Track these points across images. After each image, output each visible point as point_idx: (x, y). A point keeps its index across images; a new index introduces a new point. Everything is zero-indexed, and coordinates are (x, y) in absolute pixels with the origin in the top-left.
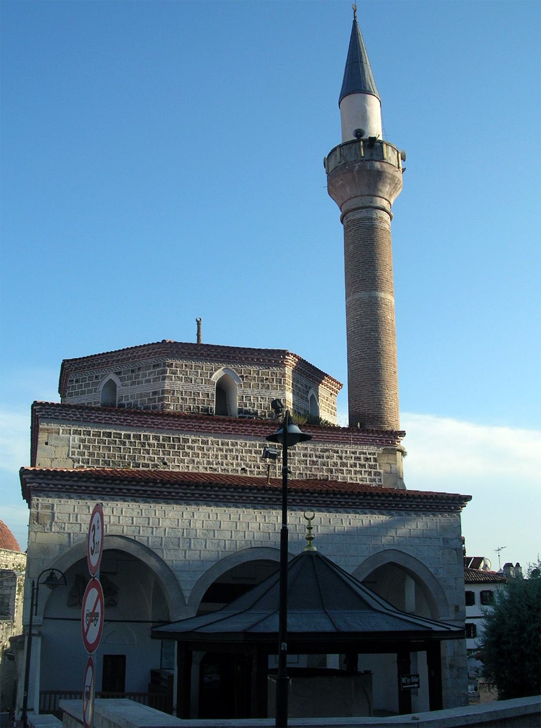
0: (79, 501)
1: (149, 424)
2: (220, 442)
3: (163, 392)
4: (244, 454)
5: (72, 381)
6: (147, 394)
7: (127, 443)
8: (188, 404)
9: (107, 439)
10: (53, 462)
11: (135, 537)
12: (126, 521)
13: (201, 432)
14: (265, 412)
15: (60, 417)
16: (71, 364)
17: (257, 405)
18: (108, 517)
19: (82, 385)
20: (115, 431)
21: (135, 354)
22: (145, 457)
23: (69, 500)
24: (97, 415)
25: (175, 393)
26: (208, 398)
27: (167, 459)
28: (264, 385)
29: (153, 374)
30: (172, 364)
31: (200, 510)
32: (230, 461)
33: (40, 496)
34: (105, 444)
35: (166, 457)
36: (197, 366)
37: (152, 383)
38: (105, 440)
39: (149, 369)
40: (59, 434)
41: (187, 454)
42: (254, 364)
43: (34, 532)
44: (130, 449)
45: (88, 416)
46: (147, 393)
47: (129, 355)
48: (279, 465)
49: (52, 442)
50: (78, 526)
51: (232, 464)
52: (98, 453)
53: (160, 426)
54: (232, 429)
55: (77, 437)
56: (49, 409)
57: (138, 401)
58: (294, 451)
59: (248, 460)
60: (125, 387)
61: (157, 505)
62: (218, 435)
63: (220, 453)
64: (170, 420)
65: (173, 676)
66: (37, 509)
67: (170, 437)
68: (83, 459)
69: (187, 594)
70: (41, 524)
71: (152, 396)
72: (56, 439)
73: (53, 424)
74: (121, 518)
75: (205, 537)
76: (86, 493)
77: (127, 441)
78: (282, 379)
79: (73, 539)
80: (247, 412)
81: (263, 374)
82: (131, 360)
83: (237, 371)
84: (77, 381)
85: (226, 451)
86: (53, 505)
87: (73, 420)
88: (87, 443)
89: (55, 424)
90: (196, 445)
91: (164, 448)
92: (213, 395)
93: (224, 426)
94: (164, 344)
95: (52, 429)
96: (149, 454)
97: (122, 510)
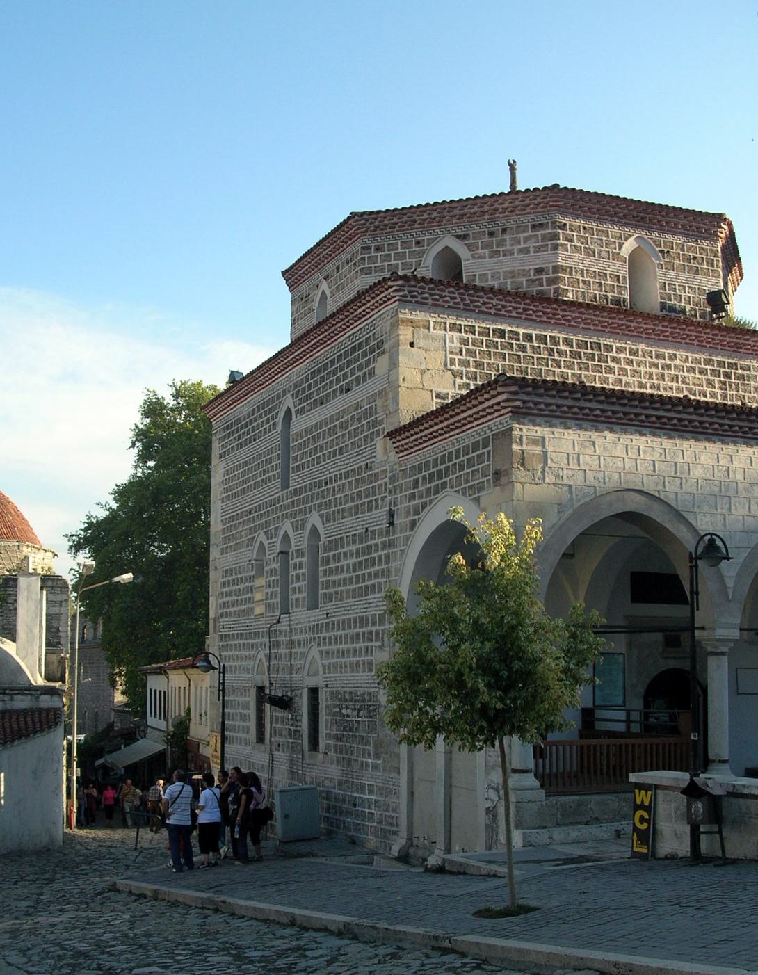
0: (578, 432)
1: (559, 319)
2: (654, 353)
3: (557, 269)
4: (686, 374)
5: (369, 248)
6: (525, 273)
7: (528, 348)
8: (592, 291)
9: (499, 340)
10: (424, 376)
11: (658, 492)
13: (628, 335)
14: (695, 310)
15: (430, 301)
16: (367, 220)
17: (685, 299)
18: (622, 459)
19: (390, 255)
20: (510, 329)
21: (496, 205)
22: (554, 372)
23: (566, 431)
24: (486, 300)
25: (574, 273)
26: (619, 282)
27: (586, 376)
28: (691, 268)
29: (534, 240)
30: (565, 224)
31: (740, 452)
32: (669, 383)
33: (524, 424)
34: (497, 349)
35: (584, 373)
36: (599, 230)
37: (532, 254)
38: (497, 342)
39: (524, 232)
40: (429, 329)
41: (611, 370)
42: (676, 232)
43: (520, 483)
44: (533, 357)
45: (472, 301)
46: (524, 270)
47: (486, 208)
48: (731, 392)
49: (420, 342)
50: (581, 473)
51: (671, 389)
52: (488, 364)
53: (573, 323)
54: (672, 333)
55: (456, 335)
56: (416, 286)
57: (506, 283)
58: (748, 372)
59: (691, 383)
60: (480, 260)
61: (684, 442)
62: (651, 342)
63: (654, 370)
64: (588, 314)
66: (522, 446)
67: (586, 342)
68: (467, 372)
69: (730, 583)
70: (529, 470)
71: (534, 275)
72: (426, 337)
73: (418, 313)
74: (638, 462)
75: (749, 495)
76: (587, 420)
77: (528, 344)
78: (715, 259)
79: (577, 495)
80: (672, 309)
81: (690, 249)
82: (487, 216)
83: (654, 242)
84: (378, 249)
85: (663, 368)
86: (543, 438)
87: (449, 307)
88: (470, 347)
89: (423, 313)
90: (622, 356)
91: (580, 358)
92: (624, 278)
93: (660, 328)
94: (556, 190)
95: (418, 321)
96: (560, 367)
97: (639, 449)
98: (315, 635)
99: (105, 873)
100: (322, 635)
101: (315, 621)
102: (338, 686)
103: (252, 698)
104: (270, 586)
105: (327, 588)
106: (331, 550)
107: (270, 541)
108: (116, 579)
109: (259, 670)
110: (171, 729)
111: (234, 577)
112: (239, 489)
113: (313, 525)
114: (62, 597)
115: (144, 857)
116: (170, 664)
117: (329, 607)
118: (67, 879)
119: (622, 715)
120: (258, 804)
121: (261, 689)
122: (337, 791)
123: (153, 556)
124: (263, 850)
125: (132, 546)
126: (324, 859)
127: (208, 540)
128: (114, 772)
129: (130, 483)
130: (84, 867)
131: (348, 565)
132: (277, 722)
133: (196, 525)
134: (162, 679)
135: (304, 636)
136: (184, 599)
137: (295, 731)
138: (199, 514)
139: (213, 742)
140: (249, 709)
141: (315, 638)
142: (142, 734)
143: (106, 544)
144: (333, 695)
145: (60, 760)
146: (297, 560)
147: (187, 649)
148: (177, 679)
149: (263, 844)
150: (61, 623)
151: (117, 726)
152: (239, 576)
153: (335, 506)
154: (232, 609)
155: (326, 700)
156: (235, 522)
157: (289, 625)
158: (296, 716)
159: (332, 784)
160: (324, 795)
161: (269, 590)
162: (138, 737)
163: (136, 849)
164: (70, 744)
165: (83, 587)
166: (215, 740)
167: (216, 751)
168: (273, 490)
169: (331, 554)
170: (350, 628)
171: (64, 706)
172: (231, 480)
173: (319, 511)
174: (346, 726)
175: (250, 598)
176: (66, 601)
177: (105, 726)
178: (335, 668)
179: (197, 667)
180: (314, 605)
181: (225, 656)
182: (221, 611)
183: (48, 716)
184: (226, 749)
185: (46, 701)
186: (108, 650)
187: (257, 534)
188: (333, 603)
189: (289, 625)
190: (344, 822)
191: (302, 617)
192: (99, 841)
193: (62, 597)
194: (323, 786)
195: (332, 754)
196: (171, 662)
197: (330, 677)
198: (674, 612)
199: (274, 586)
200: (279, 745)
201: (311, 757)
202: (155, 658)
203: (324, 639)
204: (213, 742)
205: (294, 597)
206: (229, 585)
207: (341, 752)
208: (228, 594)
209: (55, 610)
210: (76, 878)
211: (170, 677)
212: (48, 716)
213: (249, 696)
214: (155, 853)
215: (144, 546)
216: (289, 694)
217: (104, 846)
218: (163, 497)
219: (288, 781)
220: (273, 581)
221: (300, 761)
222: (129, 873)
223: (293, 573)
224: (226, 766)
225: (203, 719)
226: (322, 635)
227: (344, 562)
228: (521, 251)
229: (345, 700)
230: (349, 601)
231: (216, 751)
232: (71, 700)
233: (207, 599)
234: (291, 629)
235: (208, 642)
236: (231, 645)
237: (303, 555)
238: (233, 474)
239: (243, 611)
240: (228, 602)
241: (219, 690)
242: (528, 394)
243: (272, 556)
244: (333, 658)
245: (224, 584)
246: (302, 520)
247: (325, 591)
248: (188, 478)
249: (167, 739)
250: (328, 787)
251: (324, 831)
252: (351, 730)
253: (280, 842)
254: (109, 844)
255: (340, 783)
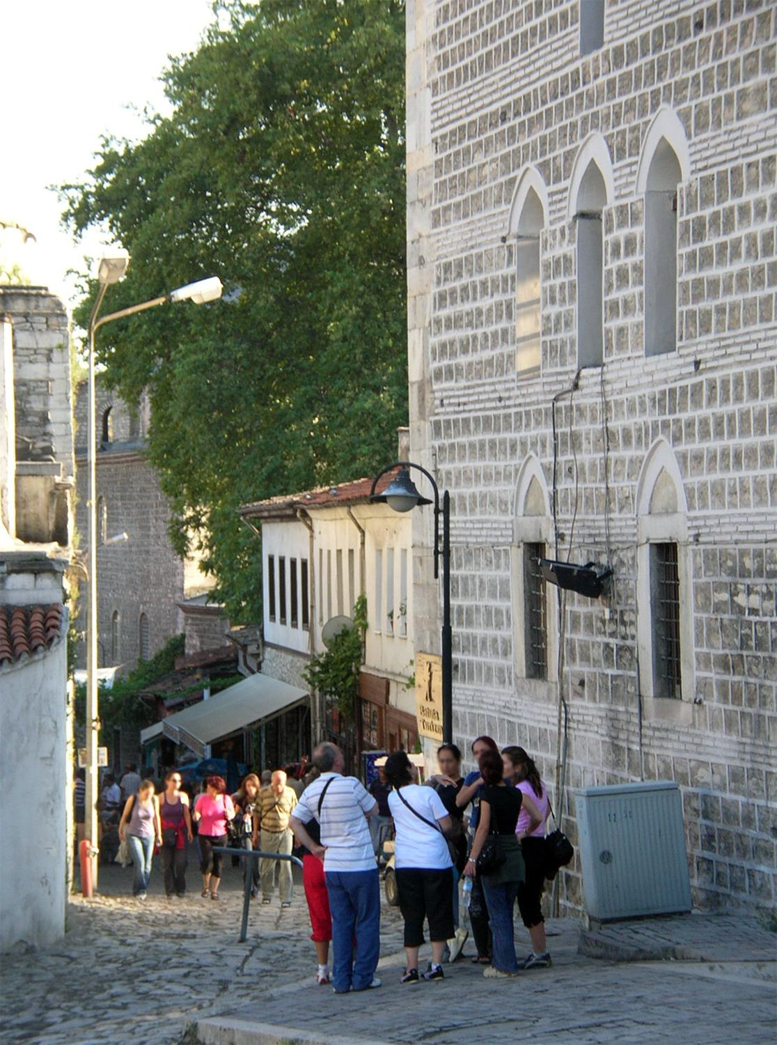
98: (667, 417)
99: (168, 1001)
100: (683, 416)
101: (666, 381)
102: (728, 538)
103: (513, 571)
104: (553, 301)
105: (697, 298)
106: (707, 201)
107: (553, 188)
108: (181, 294)
109: (531, 504)
110: (322, 648)
111: (466, 280)
112: (475, 56)
113: (663, 139)
114: (48, 340)
115: (265, 960)
116: (314, 496)
117: (703, 345)
118: (76, 1022)
120: (535, 824)
121: (535, 549)
122: (729, 796)
123: (267, 235)
124: (549, 941)
125: (214, 212)
126: (705, 966)
127: (400, 194)
128: (188, 755)
129: (205, 51)
130: (117, 988)
131: (752, 239)
132: (575, 626)
133: (368, 157)
134: (297, 530)
135: (639, 419)
136: (345, 339)
137: (620, 648)
138: (373, 127)
139: (421, 679)
140: (508, 597)
141: (666, 425)
142: (252, 663)
143: (151, 208)
144: (713, 560)
145: (57, 730)
146: (620, 234)
147: (354, 458)
148: (332, 531)
149: (549, 925)
150: (52, 402)
151: (193, 645)
152: (478, 278)
153: (721, 86)
154: (463, 360)
155: (697, 574)
156: (466, 143)
157: (603, 394)
158: (622, 613)
159: (717, 779)
160: (697, 804)
161: (553, 310)
162: (241, 668)
163: (243, 940)
164: (81, 692)
165: (102, 313)
166: (428, 672)
167: (430, 697)
168: (561, 53)
169: (707, 212)
170: (754, 395)
171: (66, 598)
172: (454, 32)
173: (677, 103)
174: (748, 637)
175: (505, 332)
176: (62, 347)
177: (163, 646)
178: (478, 476)
179: (383, 499)
180: (663, 343)
181: (448, 473)
182: (436, 365)
183: (27, 623)
184: (456, 693)
185: (24, 589)
186: (168, 466)
187: (522, 169)
188: (712, 336)
189: (603, 394)
190: (751, 873)
191: (635, 373)
192: (154, 923)
193: (48, 340)
194: (695, 783)
195: (715, 704)
196: (318, 490)
197: (705, 518)
199: (563, 301)
200: (582, 683)
201: (661, 713)
202: (276, 482)
203: (690, 424)
204: (421, 679)
205: (611, 325)
206: (453, 302)
207: (737, 699)
208: (451, 323)
209: (36, 371)
210: (99, 1019)
211: (317, 525)
212: (27, 623)
213: (507, 565)
214: (289, 950)
215: (243, 212)
216: (604, 560)
217: (167, 935)
218: (286, 87)
219: (607, 770)
220: (562, 287)
221: (637, 721)
222: (229, 1000)
223: (611, 265)
224: (456, 735)
225: (398, 623)
226: (683, 416)
227: (739, 232)
229: (744, 573)
230: (753, 328)
231: (430, 697)
232: (82, 586)
233: (401, 338)
234: (607, 403)
235: (403, 441)
236: (462, 447)
237: (635, 219)
238: (460, 18)
239: (490, 363)
240: (452, 343)
241: (436, 553)
243: (558, 226)
244: (711, 469)
245: (441, 300)
246: (633, 130)
247: (691, 307)
248: (345, 35)
249: (313, 674)
250: (705, 784)
251: (702, 896)
252: (760, 645)
253: (591, 919)
254: (178, 929)
255: (736, 776)
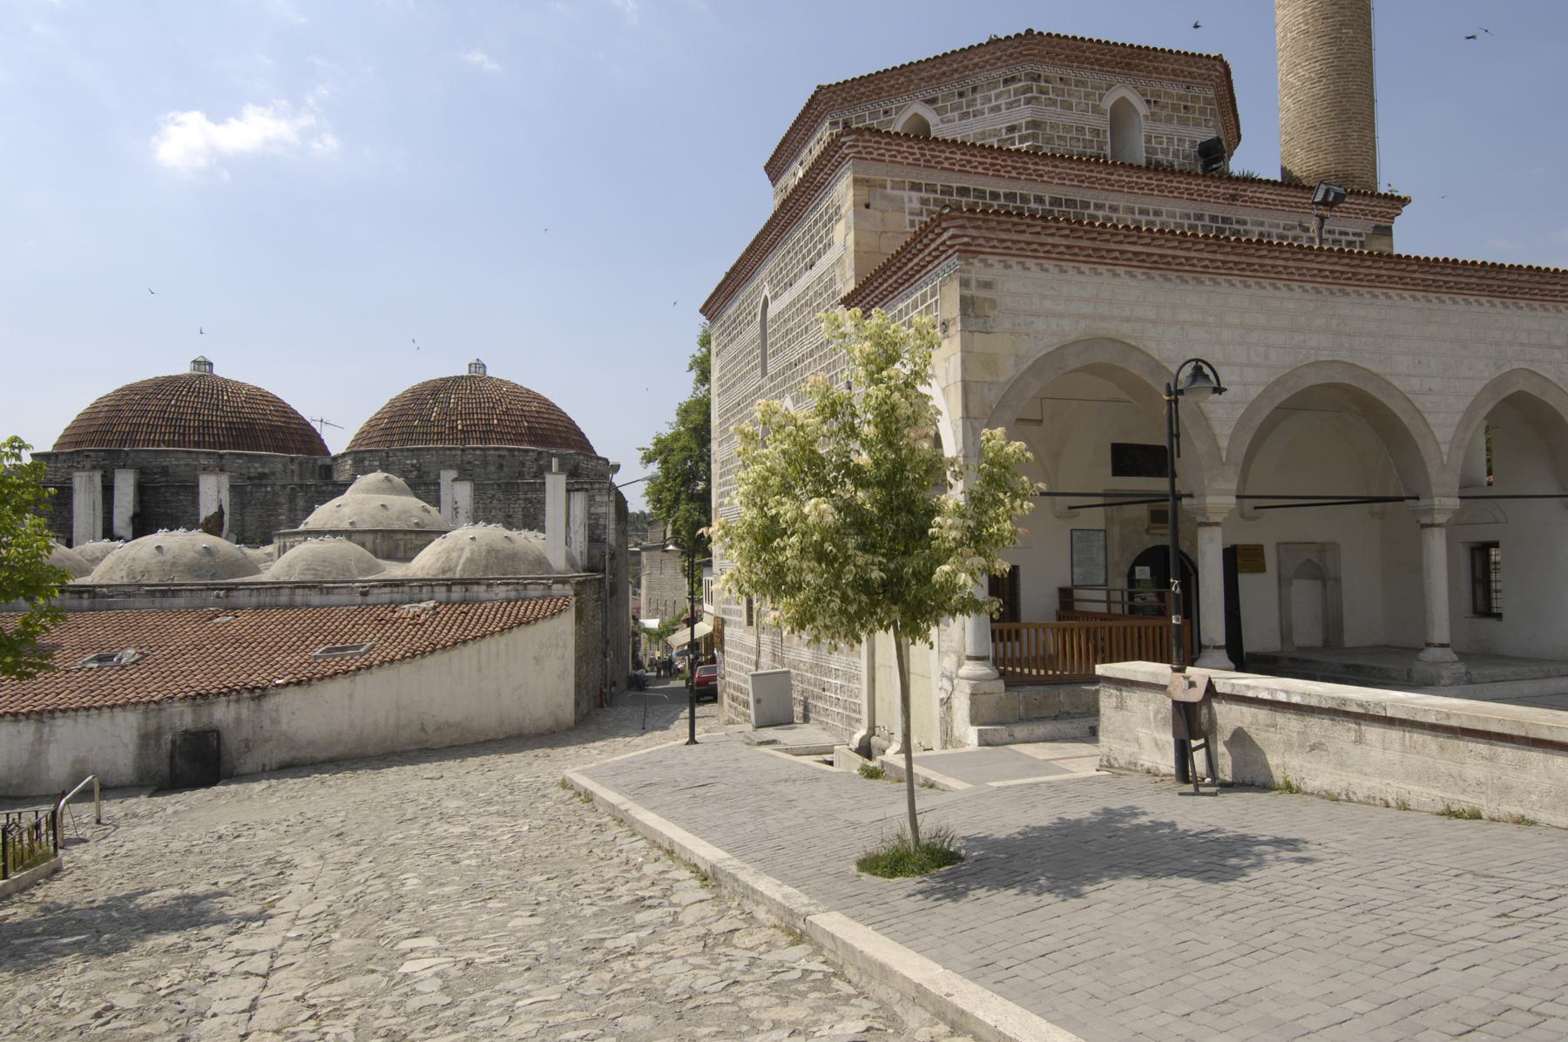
6: (996, 133)
12: (904, 341)
15: (887, 158)
55: (915, 195)
65: (1261, 555)
69: (1224, 443)
119: (1102, 595)
168: (756, 378)
198: (1160, 484)
228: (992, 110)
242: (978, 228)
